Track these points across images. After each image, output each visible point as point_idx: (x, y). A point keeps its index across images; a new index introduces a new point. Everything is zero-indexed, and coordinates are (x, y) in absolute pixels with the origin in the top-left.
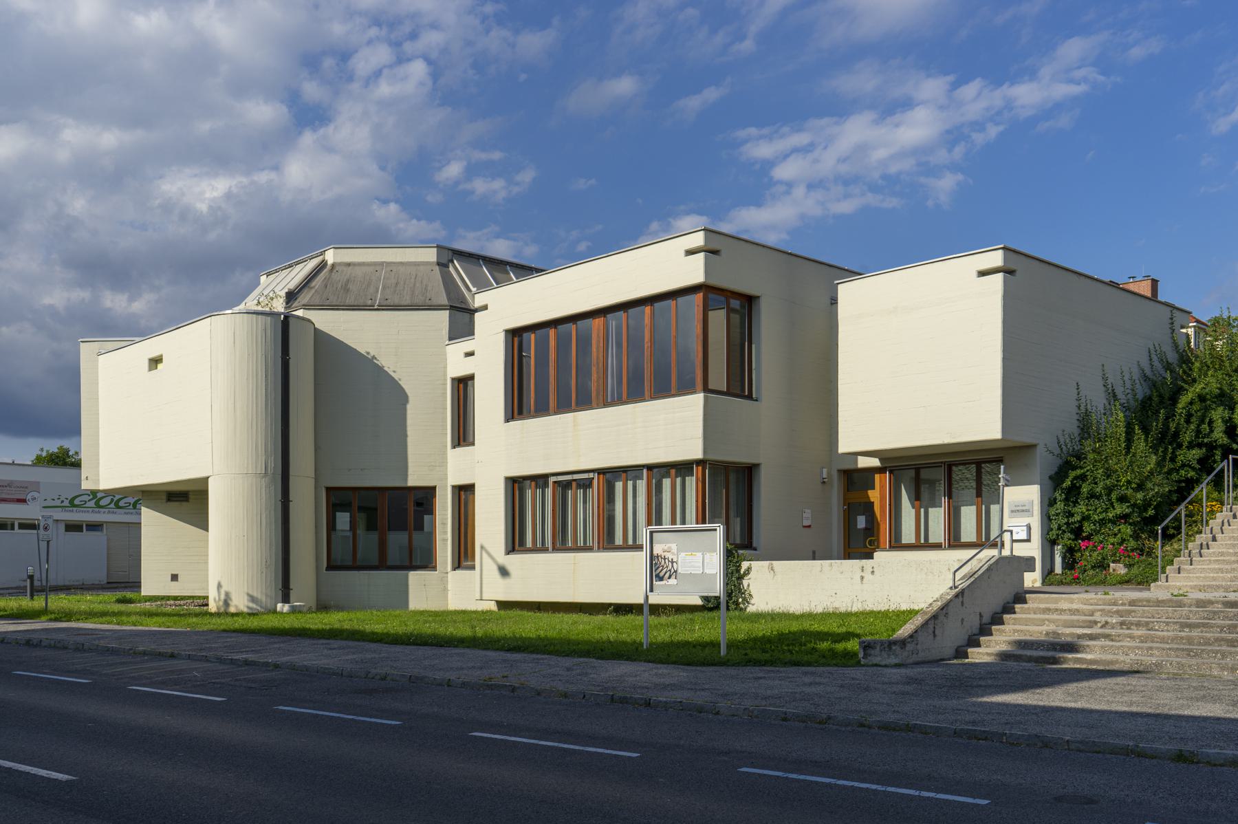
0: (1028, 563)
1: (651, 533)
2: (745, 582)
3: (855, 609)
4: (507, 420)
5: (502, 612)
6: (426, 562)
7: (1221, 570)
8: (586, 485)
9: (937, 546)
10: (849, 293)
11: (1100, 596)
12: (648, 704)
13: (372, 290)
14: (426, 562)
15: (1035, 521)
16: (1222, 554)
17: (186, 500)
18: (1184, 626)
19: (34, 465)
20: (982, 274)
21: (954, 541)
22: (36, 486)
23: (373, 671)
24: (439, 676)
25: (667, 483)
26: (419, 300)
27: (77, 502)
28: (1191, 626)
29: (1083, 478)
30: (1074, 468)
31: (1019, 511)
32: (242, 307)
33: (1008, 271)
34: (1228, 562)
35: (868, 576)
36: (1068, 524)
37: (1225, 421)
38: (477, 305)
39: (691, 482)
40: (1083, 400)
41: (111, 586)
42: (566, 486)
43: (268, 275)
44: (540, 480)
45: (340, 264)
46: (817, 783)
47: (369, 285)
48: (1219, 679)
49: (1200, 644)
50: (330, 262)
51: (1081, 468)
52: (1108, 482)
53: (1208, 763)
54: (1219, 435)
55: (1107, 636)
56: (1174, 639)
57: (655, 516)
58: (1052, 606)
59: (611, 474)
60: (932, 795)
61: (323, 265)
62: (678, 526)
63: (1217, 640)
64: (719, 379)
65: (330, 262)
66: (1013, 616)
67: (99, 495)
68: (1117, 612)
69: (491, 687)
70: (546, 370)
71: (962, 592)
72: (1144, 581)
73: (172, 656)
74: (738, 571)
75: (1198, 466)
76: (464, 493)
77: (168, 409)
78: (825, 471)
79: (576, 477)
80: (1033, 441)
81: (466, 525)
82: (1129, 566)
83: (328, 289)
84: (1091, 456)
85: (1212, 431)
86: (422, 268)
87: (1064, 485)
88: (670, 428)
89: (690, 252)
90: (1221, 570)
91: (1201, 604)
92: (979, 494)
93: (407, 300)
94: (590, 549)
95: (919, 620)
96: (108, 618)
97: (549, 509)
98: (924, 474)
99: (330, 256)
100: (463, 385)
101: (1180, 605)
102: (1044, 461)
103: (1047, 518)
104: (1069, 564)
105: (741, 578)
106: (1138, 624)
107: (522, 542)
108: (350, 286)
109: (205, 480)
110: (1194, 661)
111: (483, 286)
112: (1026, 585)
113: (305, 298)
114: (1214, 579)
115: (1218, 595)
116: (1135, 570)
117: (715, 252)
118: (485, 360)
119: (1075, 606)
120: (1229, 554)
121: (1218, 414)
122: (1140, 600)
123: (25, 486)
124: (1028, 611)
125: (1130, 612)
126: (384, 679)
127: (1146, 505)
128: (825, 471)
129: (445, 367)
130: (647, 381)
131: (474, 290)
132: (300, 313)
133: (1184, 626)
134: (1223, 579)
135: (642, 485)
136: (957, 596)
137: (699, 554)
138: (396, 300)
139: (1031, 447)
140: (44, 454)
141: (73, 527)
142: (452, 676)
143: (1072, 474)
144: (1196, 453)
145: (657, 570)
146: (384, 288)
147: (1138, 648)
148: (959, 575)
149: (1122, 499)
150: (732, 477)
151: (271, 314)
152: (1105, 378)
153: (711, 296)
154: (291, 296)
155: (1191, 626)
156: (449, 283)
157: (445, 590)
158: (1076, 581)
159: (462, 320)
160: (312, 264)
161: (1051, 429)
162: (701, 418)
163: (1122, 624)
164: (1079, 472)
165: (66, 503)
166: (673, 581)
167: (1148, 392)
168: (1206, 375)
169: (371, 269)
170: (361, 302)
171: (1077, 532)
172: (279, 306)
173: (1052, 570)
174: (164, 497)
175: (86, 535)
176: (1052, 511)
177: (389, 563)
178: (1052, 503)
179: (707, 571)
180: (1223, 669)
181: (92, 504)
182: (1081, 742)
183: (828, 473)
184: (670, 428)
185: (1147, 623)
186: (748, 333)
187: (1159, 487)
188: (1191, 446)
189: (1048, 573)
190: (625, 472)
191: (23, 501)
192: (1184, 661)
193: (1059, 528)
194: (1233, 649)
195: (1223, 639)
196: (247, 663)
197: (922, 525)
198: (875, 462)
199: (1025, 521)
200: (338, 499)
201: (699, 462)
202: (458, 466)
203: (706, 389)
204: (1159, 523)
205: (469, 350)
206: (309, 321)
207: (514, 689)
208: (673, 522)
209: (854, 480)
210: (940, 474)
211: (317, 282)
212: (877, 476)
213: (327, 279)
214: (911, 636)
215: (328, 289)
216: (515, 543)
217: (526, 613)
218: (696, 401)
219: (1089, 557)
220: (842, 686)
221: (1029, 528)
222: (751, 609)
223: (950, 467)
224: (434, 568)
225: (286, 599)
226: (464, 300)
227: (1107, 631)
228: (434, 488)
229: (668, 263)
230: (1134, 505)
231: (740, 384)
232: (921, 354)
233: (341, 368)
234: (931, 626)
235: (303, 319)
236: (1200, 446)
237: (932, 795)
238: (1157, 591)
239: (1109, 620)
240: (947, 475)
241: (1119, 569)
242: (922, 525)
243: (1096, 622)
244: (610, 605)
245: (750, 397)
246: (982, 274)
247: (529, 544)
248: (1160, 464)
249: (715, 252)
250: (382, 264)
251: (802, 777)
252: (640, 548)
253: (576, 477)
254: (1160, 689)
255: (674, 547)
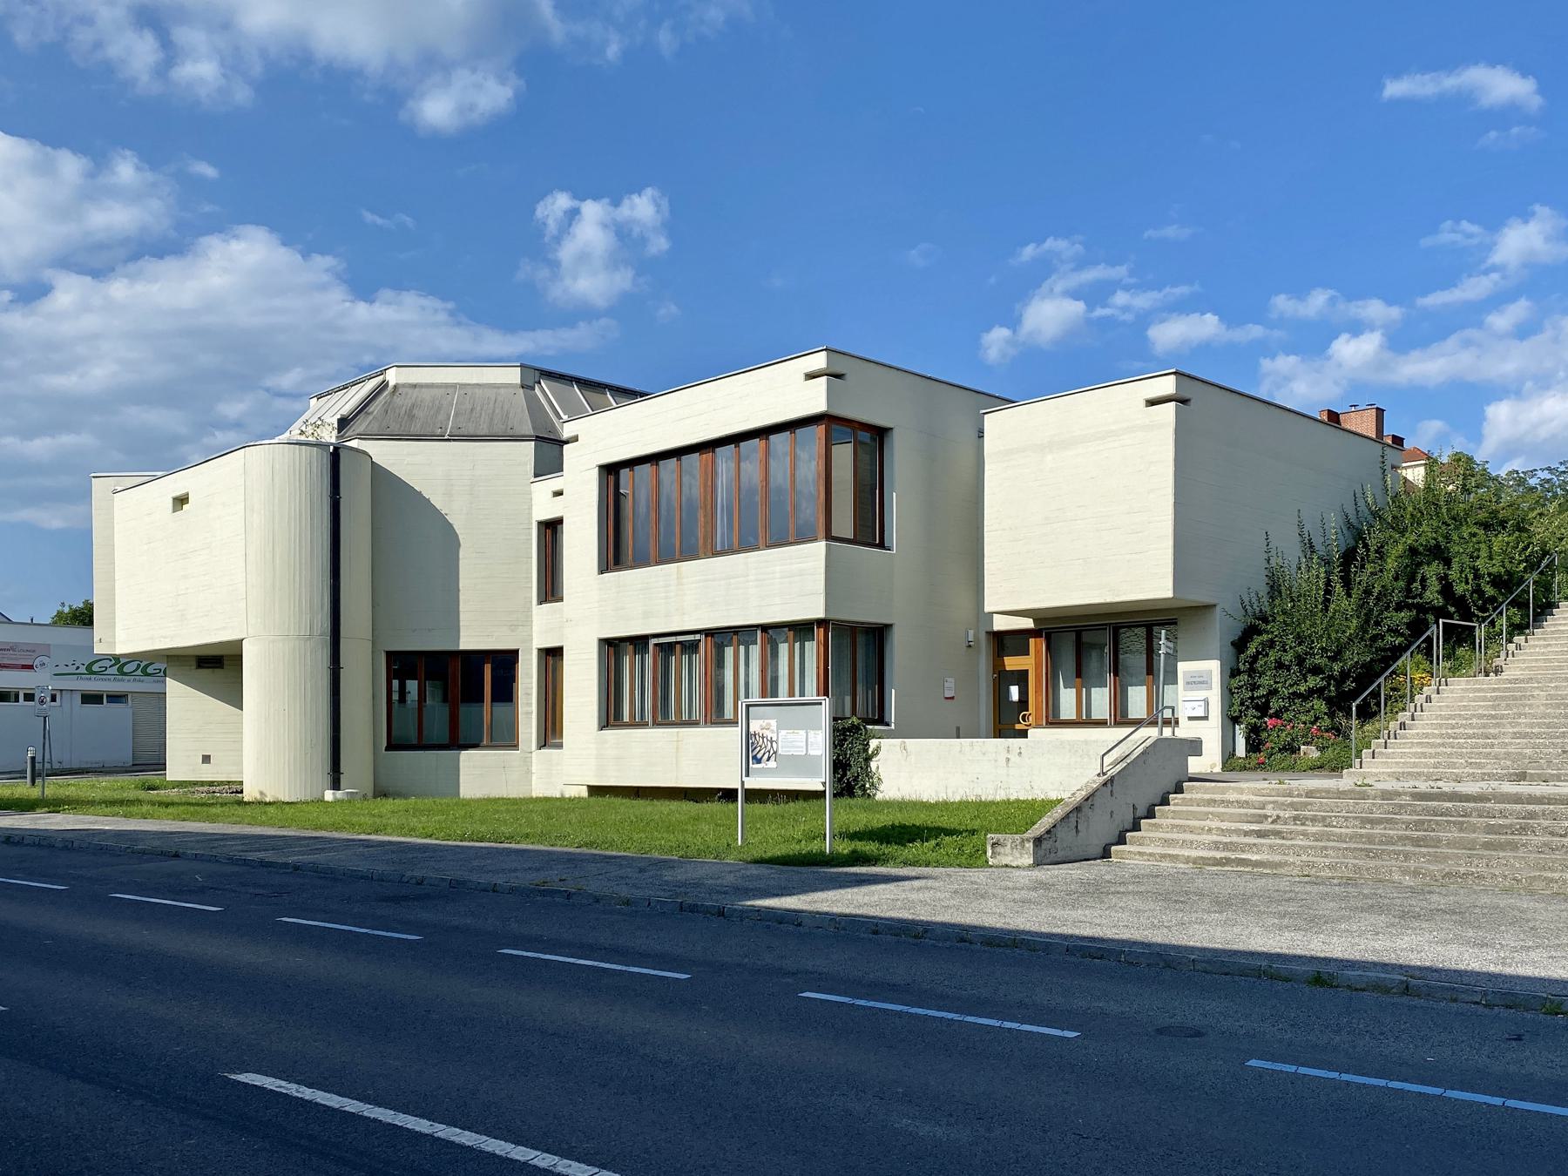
0: (1195, 747)
1: (748, 706)
2: (873, 765)
3: (998, 798)
4: (601, 572)
5: (593, 799)
6: (507, 739)
7: (1424, 755)
8: (692, 647)
9: (1101, 723)
10: (995, 423)
11: (1274, 785)
12: (721, 913)
13: (441, 417)
14: (507, 739)
15: (1215, 695)
16: (1427, 736)
17: (217, 666)
18: (1365, 821)
19: (54, 624)
20: (1152, 403)
21: (1120, 717)
22: (45, 650)
23: (409, 874)
24: (484, 879)
25: (783, 649)
26: (499, 429)
27: (95, 668)
28: (1374, 822)
29: (1272, 644)
30: (1260, 633)
31: (1198, 682)
32: (284, 437)
33: (1182, 401)
34: (1432, 745)
35: (1014, 758)
36: (1252, 698)
37: (1440, 579)
38: (566, 435)
39: (811, 648)
40: (1273, 553)
41: (137, 767)
42: (666, 650)
43: (319, 397)
44: (639, 642)
45: (404, 385)
46: (885, 1010)
47: (439, 409)
48: (1398, 886)
49: (1381, 843)
50: (391, 384)
51: (1268, 633)
52: (1299, 649)
53: (1349, 987)
54: (1432, 595)
55: (1277, 834)
56: (1352, 837)
57: (769, 687)
58: (1218, 797)
59: (721, 636)
60: (1014, 1025)
61: (384, 386)
62: (797, 698)
63: (1400, 838)
64: (844, 523)
65: (391, 384)
66: (1166, 808)
67: (123, 661)
68: (1292, 805)
69: (544, 893)
70: (642, 516)
71: (1112, 780)
72: (1336, 767)
73: (176, 856)
74: (866, 750)
75: (1407, 632)
76: (552, 656)
77: (196, 558)
78: (971, 633)
79: (680, 638)
80: (1212, 601)
81: (554, 694)
82: (1322, 749)
83: (389, 414)
84: (1280, 618)
85: (1424, 587)
86: (502, 391)
87: (1246, 654)
88: (787, 582)
89: (811, 376)
90: (1424, 755)
91: (1387, 795)
92: (1079, 674)
93: (483, 429)
94: (695, 724)
95: (1058, 812)
96: (116, 809)
97: (650, 677)
98: (1086, 637)
99: (392, 377)
100: (551, 529)
101: (1364, 796)
102: (1221, 629)
103: (1228, 692)
104: (1253, 746)
105: (868, 759)
106: (1314, 820)
107: (666, 713)
108: (415, 411)
109: (239, 644)
110: (1372, 863)
111: (576, 413)
112: (1190, 770)
113: (360, 425)
114: (1415, 765)
115: (1408, 785)
116: (1329, 753)
117: (839, 376)
118: (577, 501)
119: (1244, 798)
120: (1434, 736)
121: (1432, 571)
122: (1318, 791)
123: (32, 650)
124: (1190, 802)
125: (1306, 804)
126: (420, 883)
127: (1344, 675)
128: (971, 633)
129: (530, 508)
130: (763, 528)
131: (565, 417)
132: (354, 444)
133: (1365, 821)
134: (1426, 766)
135: (755, 651)
136: (1105, 784)
137: (802, 732)
138: (470, 429)
139: (1212, 607)
140: (66, 610)
141: (91, 698)
142: (500, 880)
143: (1258, 640)
144: (1405, 616)
145: (753, 752)
146: (456, 414)
147: (1311, 847)
148: (1108, 760)
149: (1316, 670)
150: (861, 639)
151: (320, 445)
152: (1301, 526)
153: (834, 426)
154: (343, 423)
155: (1374, 822)
156: (534, 408)
157: (529, 772)
158: (1260, 766)
159: (550, 453)
160: (370, 385)
161: (1233, 590)
162: (823, 570)
163: (1295, 818)
164: (1265, 637)
165: (83, 670)
166: (772, 764)
167: (1352, 543)
168: (1420, 524)
169: (442, 391)
170: (428, 431)
171: (1263, 709)
172: (329, 436)
173: (1233, 754)
174: (194, 663)
175: (106, 708)
176: (1235, 683)
177: (461, 742)
178: (1235, 673)
179: (811, 752)
180: (1404, 872)
181: (114, 670)
182: (1208, 962)
183: (975, 636)
184: (787, 582)
185: (1324, 818)
186: (861, 470)
187: (1356, 656)
188: (1399, 608)
189: (1229, 757)
190: (736, 633)
191: (30, 667)
192: (1361, 863)
193: (1242, 704)
194: (1417, 849)
195: (1407, 838)
196: (263, 864)
197: (1084, 704)
198: (1028, 623)
199: (1202, 694)
200: (402, 665)
201: (821, 623)
202: (543, 627)
203: (829, 537)
204: (1355, 695)
205: (557, 488)
206: (365, 453)
207: (569, 895)
208: (791, 694)
209: (1005, 643)
210: (1107, 637)
211: (375, 408)
212: (1032, 641)
213: (388, 404)
214: (1048, 832)
215: (389, 414)
216: (611, 717)
217: (617, 801)
218: (819, 548)
219: (1272, 741)
220: (956, 892)
221: (1206, 702)
222: (879, 796)
223: (1116, 630)
224: (515, 747)
225: (336, 785)
226: (553, 429)
227: (1278, 827)
228: (517, 651)
229: (788, 389)
230: (1331, 677)
231: (870, 529)
232: (1079, 497)
233: (401, 510)
234: (1073, 819)
235: (357, 450)
236: (1410, 607)
237: (1014, 1025)
238: (1347, 781)
239: (1282, 814)
240: (1100, 644)
241: (1311, 752)
242: (1084, 704)
243: (1266, 817)
244: (719, 790)
245: (882, 545)
246: (1152, 403)
247: (626, 718)
248: (1363, 628)
249: (839, 376)
250: (454, 386)
251: (872, 1004)
252: (734, 723)
253: (680, 638)
254: (1324, 896)
255: (773, 723)
